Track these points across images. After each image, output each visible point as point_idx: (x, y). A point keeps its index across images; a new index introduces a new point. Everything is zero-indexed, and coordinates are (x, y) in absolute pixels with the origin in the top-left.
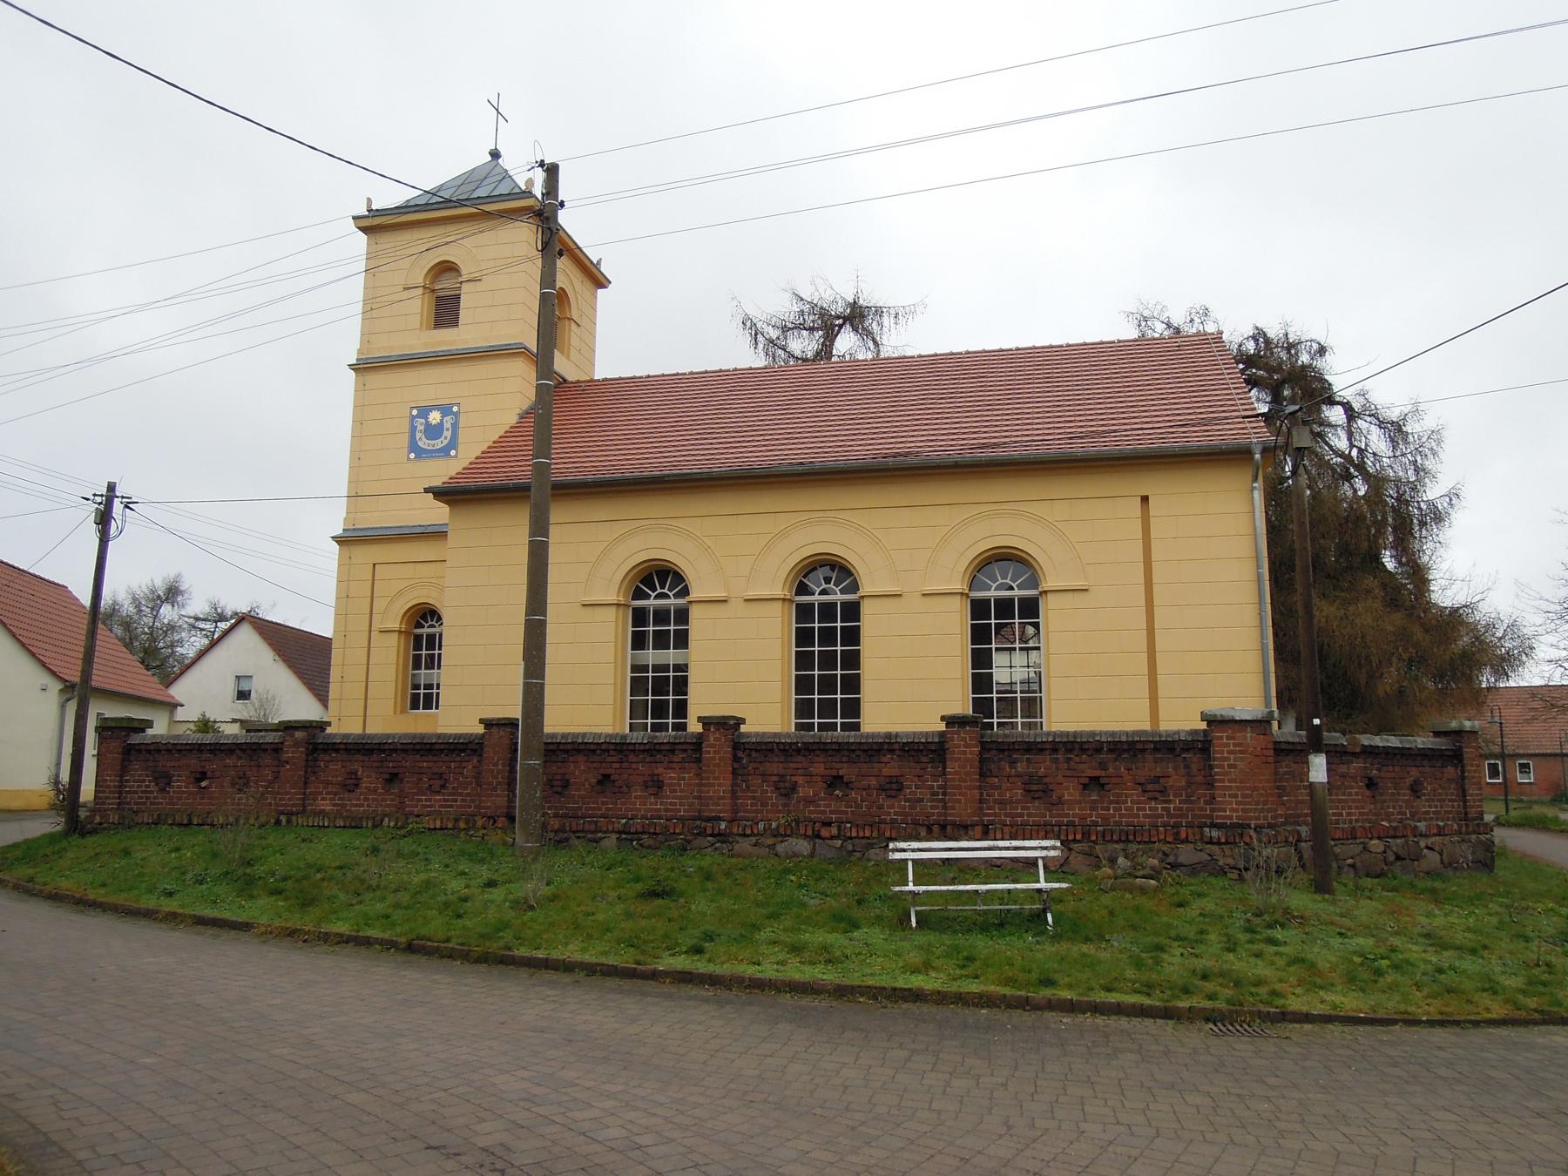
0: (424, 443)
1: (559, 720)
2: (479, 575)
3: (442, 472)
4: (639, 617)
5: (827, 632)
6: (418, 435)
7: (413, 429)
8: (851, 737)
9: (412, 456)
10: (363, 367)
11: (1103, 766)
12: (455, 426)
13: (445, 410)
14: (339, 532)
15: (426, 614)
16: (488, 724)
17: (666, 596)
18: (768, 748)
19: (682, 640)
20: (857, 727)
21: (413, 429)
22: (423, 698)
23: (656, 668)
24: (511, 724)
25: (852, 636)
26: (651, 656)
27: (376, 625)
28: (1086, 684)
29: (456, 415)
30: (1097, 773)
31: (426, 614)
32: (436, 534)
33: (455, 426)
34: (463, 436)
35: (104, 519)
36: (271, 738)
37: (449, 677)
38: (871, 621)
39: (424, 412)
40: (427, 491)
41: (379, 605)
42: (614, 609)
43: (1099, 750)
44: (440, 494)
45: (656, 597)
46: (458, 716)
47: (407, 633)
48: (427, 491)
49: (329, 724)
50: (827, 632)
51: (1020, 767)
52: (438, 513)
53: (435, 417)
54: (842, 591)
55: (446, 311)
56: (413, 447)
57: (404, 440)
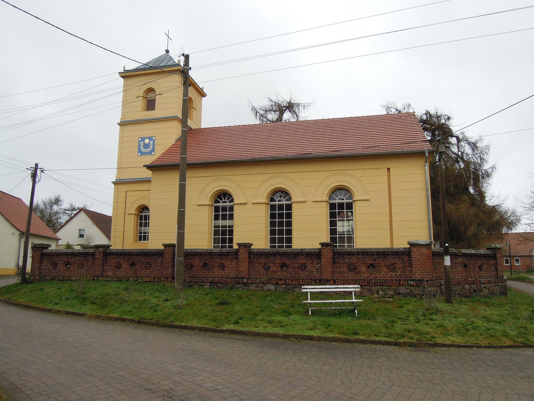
0: (143, 150)
1: (189, 244)
2: (162, 195)
3: (150, 160)
4: (217, 209)
5: (281, 214)
6: (141, 147)
7: (139, 145)
8: (289, 250)
9: (139, 154)
10: (122, 124)
11: (374, 260)
12: (154, 144)
13: (150, 139)
14: (114, 180)
15: (144, 208)
16: (165, 246)
17: (225, 202)
18: (260, 254)
19: (231, 217)
20: (291, 247)
21: (139, 145)
22: (143, 237)
23: (222, 227)
24: (173, 246)
25: (289, 216)
26: (221, 222)
27: (127, 212)
28: (368, 232)
29: (154, 140)
30: (372, 262)
31: (144, 208)
32: (147, 181)
33: (154, 144)
34: (156, 148)
35: (34, 176)
36: (91, 250)
37: (152, 230)
38: (296, 211)
39: (143, 139)
40: (144, 166)
41: (128, 205)
42: (264, 205)
43: (373, 255)
44: (149, 167)
45: (222, 202)
46: (155, 243)
47: (137, 215)
48: (144, 166)
49: (252, 245)
50: (281, 214)
51: (346, 260)
52: (148, 174)
53: (147, 141)
54: (286, 201)
55: (150, 105)
56: (140, 151)
57: (137, 149)
